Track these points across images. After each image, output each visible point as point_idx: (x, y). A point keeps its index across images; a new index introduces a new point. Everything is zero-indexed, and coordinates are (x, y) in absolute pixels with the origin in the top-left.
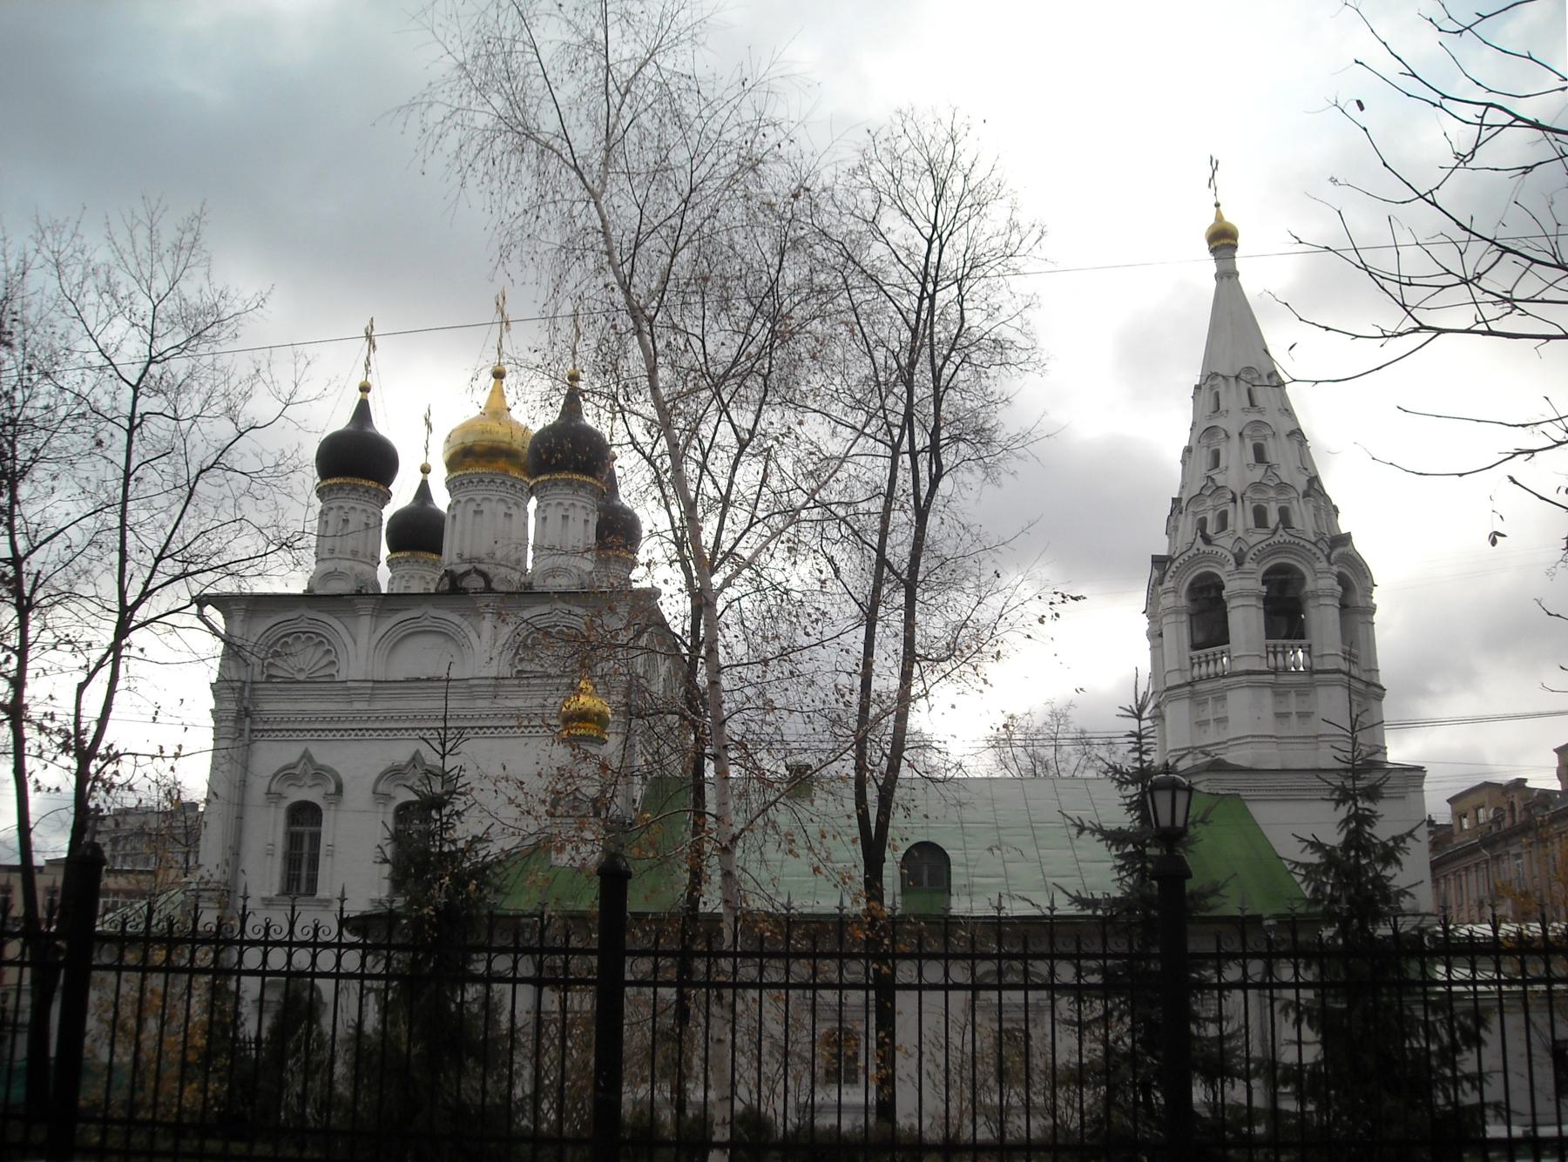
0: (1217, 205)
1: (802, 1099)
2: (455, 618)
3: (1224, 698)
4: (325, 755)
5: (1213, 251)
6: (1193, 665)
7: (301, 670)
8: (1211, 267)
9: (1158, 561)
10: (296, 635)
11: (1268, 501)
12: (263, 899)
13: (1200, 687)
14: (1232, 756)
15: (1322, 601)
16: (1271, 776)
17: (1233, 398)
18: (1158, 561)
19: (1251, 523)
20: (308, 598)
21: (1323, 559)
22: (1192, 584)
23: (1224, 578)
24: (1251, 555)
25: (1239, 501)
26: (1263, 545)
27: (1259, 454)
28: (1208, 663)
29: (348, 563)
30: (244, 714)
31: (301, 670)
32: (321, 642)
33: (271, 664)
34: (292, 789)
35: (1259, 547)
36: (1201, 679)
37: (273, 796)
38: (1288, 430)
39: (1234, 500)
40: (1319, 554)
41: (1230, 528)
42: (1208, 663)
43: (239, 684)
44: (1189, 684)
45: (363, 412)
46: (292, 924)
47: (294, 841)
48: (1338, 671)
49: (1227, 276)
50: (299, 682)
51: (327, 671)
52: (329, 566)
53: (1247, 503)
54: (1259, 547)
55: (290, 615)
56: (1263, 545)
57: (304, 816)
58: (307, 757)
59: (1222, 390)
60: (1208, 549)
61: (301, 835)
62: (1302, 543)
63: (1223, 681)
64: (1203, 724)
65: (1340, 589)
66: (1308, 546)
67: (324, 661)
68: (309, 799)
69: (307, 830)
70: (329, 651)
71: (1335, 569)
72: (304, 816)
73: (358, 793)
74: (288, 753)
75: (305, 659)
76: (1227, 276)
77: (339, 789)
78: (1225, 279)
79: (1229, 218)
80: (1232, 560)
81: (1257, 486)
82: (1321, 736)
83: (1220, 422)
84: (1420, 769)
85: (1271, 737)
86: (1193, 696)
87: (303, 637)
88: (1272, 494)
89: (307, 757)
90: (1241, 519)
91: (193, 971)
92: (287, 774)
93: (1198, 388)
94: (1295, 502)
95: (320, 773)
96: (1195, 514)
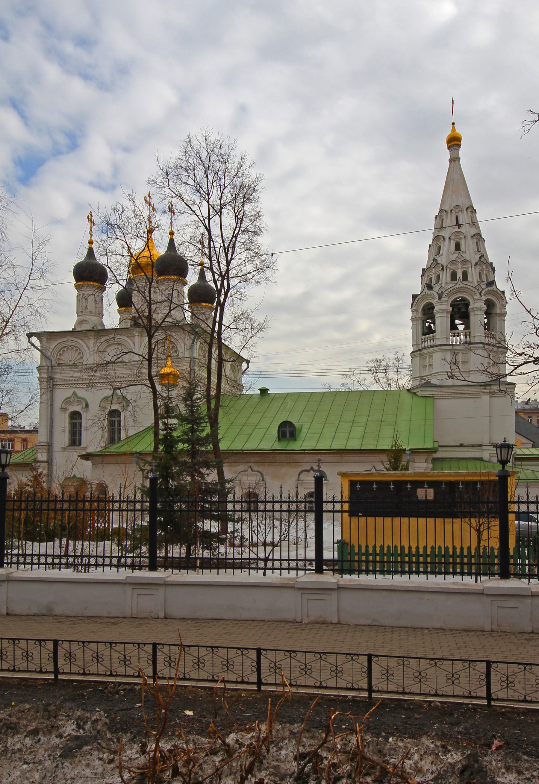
0: (453, 124)
1: (338, 537)
2: (125, 338)
3: (432, 356)
4: (81, 393)
5: (449, 148)
6: (422, 342)
7: (70, 361)
8: (447, 154)
9: (414, 297)
10: (68, 347)
11: (458, 269)
12: (62, 448)
13: (424, 351)
14: (433, 381)
15: (476, 313)
16: (447, 389)
17: (449, 221)
18: (414, 297)
19: (449, 278)
20: (74, 332)
21: (478, 294)
22: (423, 307)
23: (434, 303)
24: (445, 294)
25: (445, 270)
26: (451, 289)
27: (458, 247)
28: (430, 340)
29: (88, 317)
30: (50, 379)
31: (70, 361)
32: (77, 350)
33: (59, 359)
34: (70, 407)
35: (449, 290)
36: (425, 348)
37: (64, 409)
38: (473, 234)
39: (443, 269)
40: (476, 291)
41: (440, 282)
42: (430, 340)
43: (46, 368)
44: (419, 350)
45: (91, 252)
46: (297, 496)
47: (111, 424)
48: (481, 343)
49: (454, 160)
50: (70, 365)
51: (80, 361)
52: (82, 318)
53: (448, 270)
54: (449, 290)
55: (65, 339)
56: (451, 289)
57: (75, 416)
58: (75, 394)
59: (444, 217)
60: (429, 292)
61: (114, 421)
62: (469, 287)
63: (431, 349)
64: (424, 367)
65: (485, 307)
66: (471, 288)
67: (79, 357)
68: (77, 410)
69: (77, 421)
70: (80, 353)
71: (484, 298)
72: (75, 416)
73: (94, 408)
74: (68, 393)
75: (68, 357)
76: (454, 160)
77: (87, 406)
78: (453, 162)
79: (459, 130)
80: (437, 295)
81: (453, 262)
82: (471, 371)
83: (442, 233)
84: (514, 384)
85: (441, 372)
86: (421, 355)
87: (70, 348)
88: (459, 265)
89: (75, 394)
90: (446, 277)
91: (134, 510)
92: (67, 401)
93: (436, 216)
94: (470, 268)
95: (80, 400)
96: (428, 276)
